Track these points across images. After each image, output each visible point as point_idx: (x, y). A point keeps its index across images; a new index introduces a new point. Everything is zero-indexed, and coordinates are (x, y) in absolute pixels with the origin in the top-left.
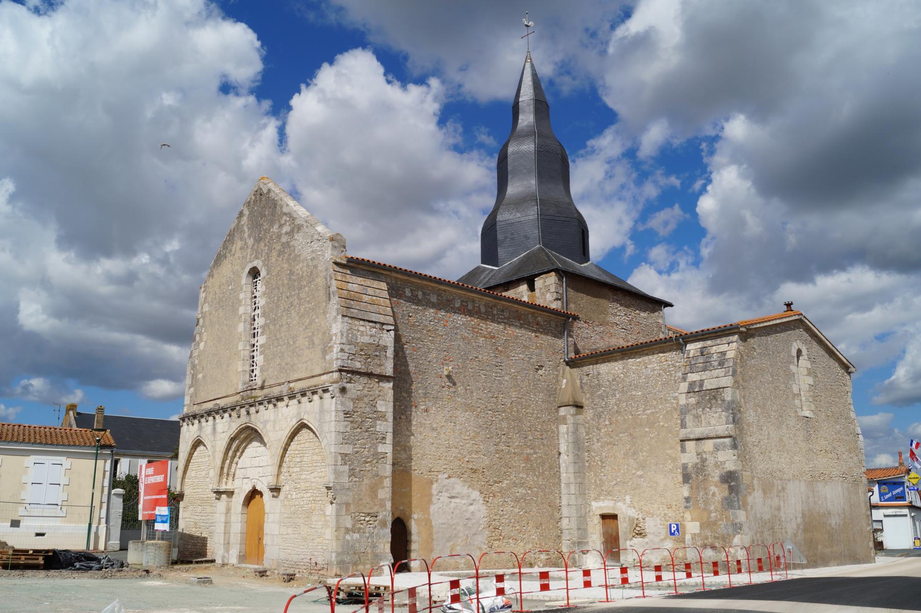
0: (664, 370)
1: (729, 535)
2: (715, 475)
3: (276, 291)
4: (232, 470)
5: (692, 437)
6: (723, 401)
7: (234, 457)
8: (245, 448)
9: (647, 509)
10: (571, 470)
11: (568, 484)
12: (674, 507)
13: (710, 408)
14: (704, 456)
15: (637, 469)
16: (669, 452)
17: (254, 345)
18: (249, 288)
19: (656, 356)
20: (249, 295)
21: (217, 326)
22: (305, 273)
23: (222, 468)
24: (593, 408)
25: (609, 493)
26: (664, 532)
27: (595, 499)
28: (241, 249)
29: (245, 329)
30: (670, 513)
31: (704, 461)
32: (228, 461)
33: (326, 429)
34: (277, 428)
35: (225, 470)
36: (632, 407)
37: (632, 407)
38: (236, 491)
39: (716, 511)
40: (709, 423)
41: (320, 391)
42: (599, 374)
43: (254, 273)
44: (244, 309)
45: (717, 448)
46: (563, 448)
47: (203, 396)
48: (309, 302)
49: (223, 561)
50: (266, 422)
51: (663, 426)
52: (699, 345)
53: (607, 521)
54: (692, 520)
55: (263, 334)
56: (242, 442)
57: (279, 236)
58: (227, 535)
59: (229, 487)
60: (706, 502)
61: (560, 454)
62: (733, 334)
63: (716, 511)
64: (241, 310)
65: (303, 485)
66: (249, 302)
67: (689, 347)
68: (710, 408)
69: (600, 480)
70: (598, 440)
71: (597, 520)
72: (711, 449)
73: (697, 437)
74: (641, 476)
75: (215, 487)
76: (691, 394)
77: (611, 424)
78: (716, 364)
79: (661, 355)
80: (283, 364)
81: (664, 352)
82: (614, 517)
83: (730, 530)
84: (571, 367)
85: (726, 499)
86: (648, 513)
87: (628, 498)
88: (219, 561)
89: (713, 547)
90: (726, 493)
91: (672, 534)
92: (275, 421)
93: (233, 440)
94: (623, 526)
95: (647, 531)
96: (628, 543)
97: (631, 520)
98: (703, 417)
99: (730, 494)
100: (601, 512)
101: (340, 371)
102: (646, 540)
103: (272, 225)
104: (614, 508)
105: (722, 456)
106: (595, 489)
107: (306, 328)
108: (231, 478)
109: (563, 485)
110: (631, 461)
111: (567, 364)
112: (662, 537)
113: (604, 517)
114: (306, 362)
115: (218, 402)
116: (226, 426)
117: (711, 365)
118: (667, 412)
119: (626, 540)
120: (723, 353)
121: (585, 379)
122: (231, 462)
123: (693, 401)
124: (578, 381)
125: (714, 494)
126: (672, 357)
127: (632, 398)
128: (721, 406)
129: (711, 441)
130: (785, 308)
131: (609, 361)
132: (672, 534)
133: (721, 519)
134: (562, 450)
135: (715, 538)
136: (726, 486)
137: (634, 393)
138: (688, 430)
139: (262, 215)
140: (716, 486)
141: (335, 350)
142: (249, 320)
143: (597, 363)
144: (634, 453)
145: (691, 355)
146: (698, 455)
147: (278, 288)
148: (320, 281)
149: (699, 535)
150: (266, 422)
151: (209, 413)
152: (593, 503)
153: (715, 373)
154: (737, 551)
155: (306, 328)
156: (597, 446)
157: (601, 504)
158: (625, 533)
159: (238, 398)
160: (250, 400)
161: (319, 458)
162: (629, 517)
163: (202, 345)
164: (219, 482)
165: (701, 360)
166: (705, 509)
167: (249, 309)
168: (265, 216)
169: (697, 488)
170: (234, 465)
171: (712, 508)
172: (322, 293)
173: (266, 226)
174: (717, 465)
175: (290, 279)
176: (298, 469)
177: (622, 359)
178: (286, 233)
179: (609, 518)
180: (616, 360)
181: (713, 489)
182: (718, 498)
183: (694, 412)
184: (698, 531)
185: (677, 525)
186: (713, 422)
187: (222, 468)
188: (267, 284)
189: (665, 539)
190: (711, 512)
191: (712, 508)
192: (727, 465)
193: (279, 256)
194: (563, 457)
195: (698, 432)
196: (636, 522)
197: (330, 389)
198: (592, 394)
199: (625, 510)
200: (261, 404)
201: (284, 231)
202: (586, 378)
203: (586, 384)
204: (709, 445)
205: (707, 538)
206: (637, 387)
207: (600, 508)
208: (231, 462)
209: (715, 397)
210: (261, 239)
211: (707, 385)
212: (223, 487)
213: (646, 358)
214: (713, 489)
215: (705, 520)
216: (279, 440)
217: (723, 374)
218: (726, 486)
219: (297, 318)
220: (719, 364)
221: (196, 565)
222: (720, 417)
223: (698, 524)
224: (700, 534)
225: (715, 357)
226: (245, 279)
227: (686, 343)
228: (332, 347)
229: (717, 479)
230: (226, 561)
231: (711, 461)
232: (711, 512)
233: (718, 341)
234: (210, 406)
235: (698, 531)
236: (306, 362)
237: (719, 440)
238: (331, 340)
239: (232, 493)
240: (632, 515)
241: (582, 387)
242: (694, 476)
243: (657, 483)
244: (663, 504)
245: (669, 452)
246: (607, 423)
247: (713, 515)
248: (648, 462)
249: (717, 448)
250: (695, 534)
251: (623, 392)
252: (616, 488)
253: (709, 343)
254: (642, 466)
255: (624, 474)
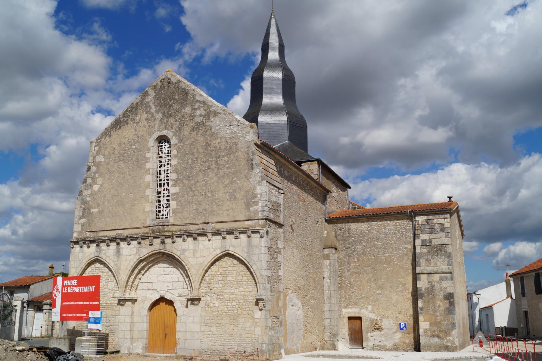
0: (399, 231)
1: (449, 330)
2: (441, 295)
3: (191, 156)
4: (136, 283)
5: (425, 272)
6: (446, 252)
7: (139, 272)
8: (150, 268)
9: (383, 314)
10: (332, 288)
11: (330, 298)
12: (403, 313)
13: (437, 256)
14: (433, 283)
15: (377, 289)
16: (400, 280)
17: (160, 193)
18: (156, 150)
19: (392, 222)
20: (155, 155)
21: (117, 175)
22: (223, 147)
23: (127, 282)
24: (345, 251)
25: (355, 304)
26: (395, 328)
27: (345, 307)
28: (146, 119)
29: (153, 180)
30: (400, 316)
31: (433, 286)
32: (133, 277)
33: (255, 258)
34: (198, 255)
35: (130, 283)
36: (374, 252)
37: (374, 252)
38: (139, 299)
39: (441, 316)
40: (436, 264)
41: (249, 233)
42: (350, 229)
43: (162, 140)
44: (152, 165)
45: (442, 279)
46: (326, 274)
47: (99, 225)
48: (228, 168)
49: (129, 351)
50: (184, 251)
51: (397, 264)
52: (425, 218)
53: (352, 321)
54: (425, 321)
55: (175, 185)
56: (148, 264)
57: (192, 117)
58: (132, 332)
59: (133, 295)
60: (434, 311)
61: (324, 278)
62: (447, 213)
63: (441, 316)
64: (148, 166)
65: (227, 297)
66: (155, 160)
67: (417, 218)
68: (437, 256)
69: (349, 295)
70: (348, 271)
71: (346, 320)
72: (438, 279)
73: (429, 272)
74: (380, 294)
75: (118, 295)
76: (424, 247)
77: (358, 261)
78: (439, 230)
79: (396, 221)
80: (200, 210)
81: (398, 220)
82: (360, 318)
83: (450, 327)
84: (328, 224)
85: (447, 309)
86: (384, 316)
87: (370, 307)
88: (124, 350)
89: (438, 337)
90: (448, 305)
91: (401, 329)
92: (196, 253)
93: (141, 261)
94: (365, 324)
95: (383, 327)
96: (369, 334)
97: (372, 321)
98: (432, 261)
99: (450, 306)
100: (349, 316)
101: (266, 219)
102: (382, 332)
103: (183, 106)
104: (359, 313)
105: (445, 284)
106: (345, 301)
107: (226, 186)
108: (134, 289)
109: (325, 298)
110: (373, 284)
111: (326, 221)
112: (394, 331)
113: (350, 318)
114: (228, 210)
115: (120, 231)
116: (131, 253)
117: (435, 230)
118: (400, 256)
119: (367, 332)
120: (443, 224)
121: (339, 232)
122: (135, 278)
123: (425, 250)
124: (334, 233)
125: (439, 306)
126: (406, 224)
127: (375, 246)
128: (444, 255)
129: (438, 275)
130: (448, 199)
131: (357, 222)
132: (401, 329)
133: (444, 320)
134: (325, 276)
135: (440, 331)
136: (448, 301)
137: (376, 243)
138: (422, 268)
139: (172, 98)
140: (441, 301)
141: (260, 204)
142: (156, 174)
143: (348, 223)
144: (375, 280)
145: (420, 224)
146: (429, 282)
147: (193, 154)
148: (241, 154)
149: (429, 330)
150: (184, 251)
151: (113, 240)
152: (343, 310)
153: (439, 235)
154: (454, 339)
155: (226, 186)
156: (347, 274)
157: (349, 310)
158: (367, 329)
159: (147, 230)
160: (160, 232)
161: (245, 278)
162: (370, 319)
163: (96, 187)
164: (125, 292)
165: (428, 227)
166: (433, 315)
167: (155, 166)
168: (175, 99)
169: (428, 302)
170: (137, 280)
171: (438, 314)
172: (243, 163)
173: (175, 106)
174: (441, 289)
175: (206, 149)
176: (221, 285)
177: (367, 221)
178: (201, 115)
179: (355, 319)
180: (363, 222)
181: (439, 303)
182: (442, 308)
183: (426, 257)
184: (428, 328)
185: (405, 324)
186: (439, 264)
187: (127, 282)
188: (179, 150)
189: (396, 332)
190: (437, 316)
191: (438, 314)
192: (448, 289)
193: (193, 129)
194: (327, 280)
195: (429, 269)
196: (375, 321)
197: (261, 231)
198: (344, 242)
199: (367, 314)
200: (178, 236)
201: (198, 113)
202: (339, 231)
203: (339, 235)
204: (436, 277)
205: (434, 332)
206: (378, 239)
207: (349, 313)
208: (135, 278)
209: (440, 250)
210: (171, 116)
211: (435, 242)
212: (127, 296)
213: (385, 222)
214: (439, 303)
215: (433, 320)
216: (201, 264)
217: (445, 236)
218: (448, 301)
219: (215, 178)
220: (441, 230)
221: (112, 355)
222: (443, 261)
223: (428, 323)
224: (430, 329)
225: (437, 226)
226: (152, 143)
227: (415, 216)
228: (257, 202)
229: (441, 297)
230: (131, 352)
231: (437, 286)
232: (437, 316)
233: (437, 217)
234: (112, 234)
235: (428, 328)
236: (228, 210)
237: (443, 275)
238: (256, 197)
239: (136, 300)
240: (372, 317)
241: (336, 237)
242: (426, 295)
243: (391, 298)
244: (395, 311)
245: (400, 280)
246: (356, 260)
247: (439, 318)
248: (385, 286)
249: (442, 279)
250: (426, 329)
251: (368, 242)
252: (361, 301)
253: (431, 217)
254: (381, 288)
255: (367, 292)
